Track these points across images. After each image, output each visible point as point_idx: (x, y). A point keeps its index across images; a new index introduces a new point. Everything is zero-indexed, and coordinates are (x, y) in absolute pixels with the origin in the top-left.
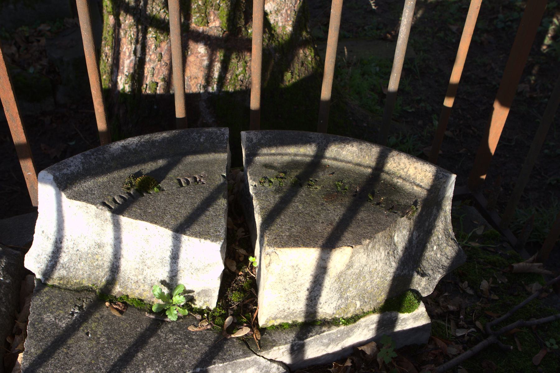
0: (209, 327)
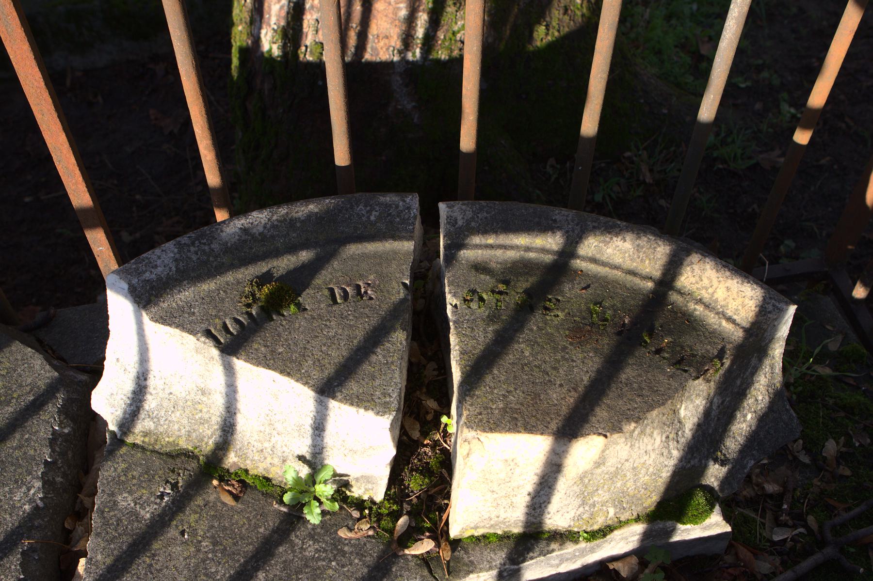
0: (371, 533)
